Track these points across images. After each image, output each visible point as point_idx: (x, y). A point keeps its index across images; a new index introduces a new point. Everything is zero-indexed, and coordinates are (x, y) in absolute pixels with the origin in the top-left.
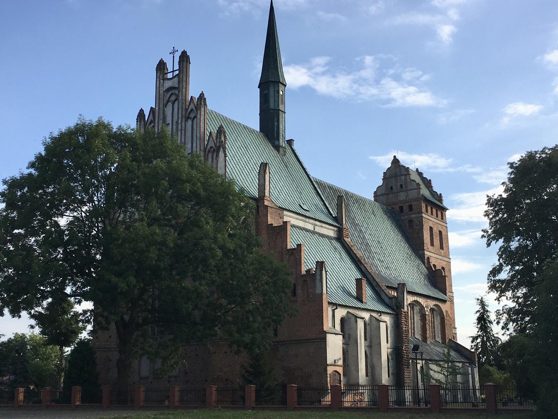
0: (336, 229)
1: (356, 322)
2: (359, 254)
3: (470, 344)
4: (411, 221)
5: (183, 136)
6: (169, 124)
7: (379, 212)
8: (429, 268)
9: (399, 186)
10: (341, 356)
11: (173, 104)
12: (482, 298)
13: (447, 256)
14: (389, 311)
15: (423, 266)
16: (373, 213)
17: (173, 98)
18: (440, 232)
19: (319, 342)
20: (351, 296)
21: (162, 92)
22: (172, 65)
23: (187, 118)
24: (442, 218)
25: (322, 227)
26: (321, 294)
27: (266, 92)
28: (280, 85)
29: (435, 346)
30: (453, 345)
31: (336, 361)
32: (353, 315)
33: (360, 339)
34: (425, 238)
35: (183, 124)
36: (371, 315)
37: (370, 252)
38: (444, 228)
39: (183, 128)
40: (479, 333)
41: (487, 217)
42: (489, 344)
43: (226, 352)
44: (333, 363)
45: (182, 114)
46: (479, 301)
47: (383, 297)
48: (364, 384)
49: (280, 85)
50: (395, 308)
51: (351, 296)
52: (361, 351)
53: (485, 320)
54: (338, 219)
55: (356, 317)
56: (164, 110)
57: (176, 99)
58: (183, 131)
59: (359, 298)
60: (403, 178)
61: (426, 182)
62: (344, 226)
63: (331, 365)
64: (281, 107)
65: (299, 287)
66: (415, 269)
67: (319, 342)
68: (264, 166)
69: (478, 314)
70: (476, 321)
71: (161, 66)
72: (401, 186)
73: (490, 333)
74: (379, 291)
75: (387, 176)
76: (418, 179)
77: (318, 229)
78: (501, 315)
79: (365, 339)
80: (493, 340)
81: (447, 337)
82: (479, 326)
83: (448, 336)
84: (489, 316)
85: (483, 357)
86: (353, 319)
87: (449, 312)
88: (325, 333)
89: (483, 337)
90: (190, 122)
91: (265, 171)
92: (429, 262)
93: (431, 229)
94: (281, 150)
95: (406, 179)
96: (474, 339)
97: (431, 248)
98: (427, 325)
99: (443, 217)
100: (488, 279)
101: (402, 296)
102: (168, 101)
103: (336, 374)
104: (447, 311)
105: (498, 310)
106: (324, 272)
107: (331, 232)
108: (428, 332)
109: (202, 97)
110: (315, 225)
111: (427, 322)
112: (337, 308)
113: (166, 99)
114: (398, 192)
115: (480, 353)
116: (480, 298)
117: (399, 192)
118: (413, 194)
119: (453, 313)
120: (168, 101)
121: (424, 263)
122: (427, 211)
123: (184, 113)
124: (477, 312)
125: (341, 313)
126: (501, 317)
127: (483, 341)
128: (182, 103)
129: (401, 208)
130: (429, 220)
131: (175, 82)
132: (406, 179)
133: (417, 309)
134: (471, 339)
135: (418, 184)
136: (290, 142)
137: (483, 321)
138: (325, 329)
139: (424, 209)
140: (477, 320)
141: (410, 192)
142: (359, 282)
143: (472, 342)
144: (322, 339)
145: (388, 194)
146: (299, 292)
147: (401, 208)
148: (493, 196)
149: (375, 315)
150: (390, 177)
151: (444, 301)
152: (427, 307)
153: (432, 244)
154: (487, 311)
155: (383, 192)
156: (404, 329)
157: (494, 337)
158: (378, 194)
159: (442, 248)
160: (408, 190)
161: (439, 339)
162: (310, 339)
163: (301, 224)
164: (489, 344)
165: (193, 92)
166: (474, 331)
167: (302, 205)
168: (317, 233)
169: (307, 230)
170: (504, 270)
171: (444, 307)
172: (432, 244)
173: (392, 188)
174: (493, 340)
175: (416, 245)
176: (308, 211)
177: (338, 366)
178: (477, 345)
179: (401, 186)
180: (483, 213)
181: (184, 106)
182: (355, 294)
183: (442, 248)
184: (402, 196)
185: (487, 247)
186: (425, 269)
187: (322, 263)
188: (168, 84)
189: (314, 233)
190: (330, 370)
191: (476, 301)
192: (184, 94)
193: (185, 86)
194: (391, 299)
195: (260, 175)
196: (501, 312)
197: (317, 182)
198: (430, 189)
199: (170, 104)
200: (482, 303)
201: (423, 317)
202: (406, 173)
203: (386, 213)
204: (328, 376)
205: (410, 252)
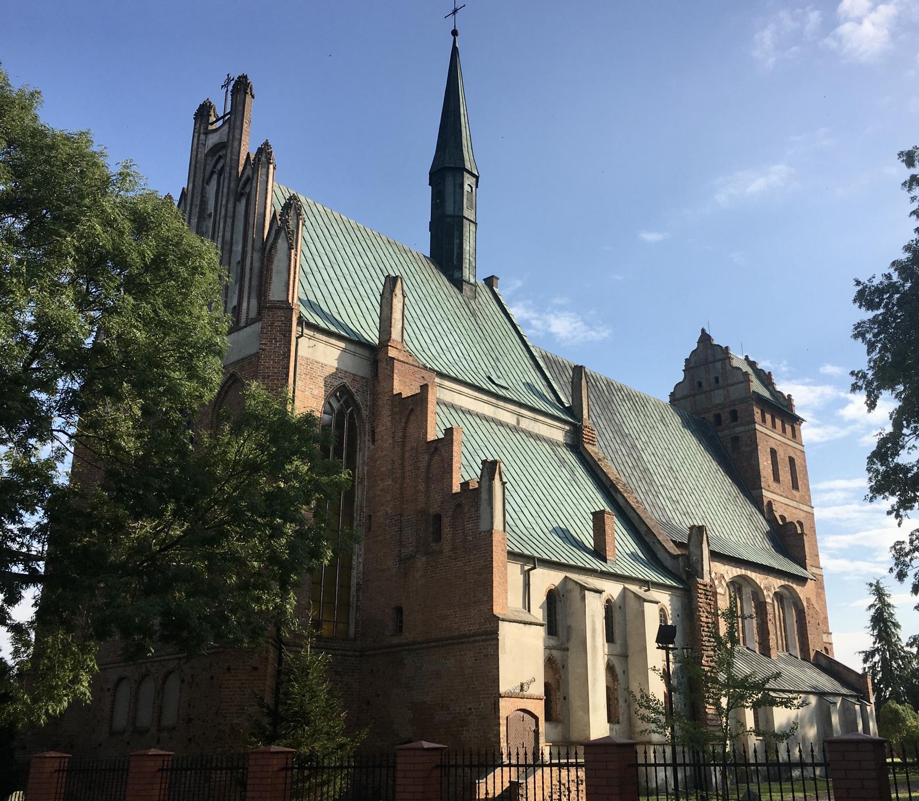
0: (567, 428)
1: (583, 598)
2: (611, 469)
3: (862, 665)
4: (736, 439)
5: (228, 229)
6: (210, 215)
7: (676, 421)
8: (770, 518)
9: (712, 379)
11: (220, 175)
12: (878, 582)
13: (807, 501)
14: (668, 582)
15: (761, 517)
16: (662, 419)
18: (792, 461)
19: (484, 641)
20: (580, 546)
21: (201, 156)
24: (794, 436)
25: (536, 420)
26: (490, 532)
28: (466, 175)
29: (787, 663)
30: (823, 662)
31: (525, 687)
32: (577, 583)
33: (594, 637)
34: (761, 467)
35: (230, 206)
36: (625, 588)
37: (651, 483)
38: (799, 453)
39: (230, 214)
40: (877, 645)
41: (860, 340)
42: (895, 665)
43: (255, 669)
44: (518, 691)
45: (229, 187)
46: (874, 588)
47: (661, 555)
49: (466, 175)
50: (684, 577)
51: (580, 546)
52: (594, 666)
53: (885, 621)
54: (574, 411)
55: (583, 588)
56: (203, 189)
58: (229, 220)
59: (599, 552)
60: (719, 365)
61: (764, 377)
62: (587, 422)
63: (510, 696)
64: (467, 213)
65: (446, 521)
66: (745, 522)
67: (484, 641)
68: (391, 282)
69: (873, 611)
70: (869, 624)
72: (717, 380)
73: (896, 645)
74: (651, 544)
75: (691, 365)
76: (746, 368)
77: (525, 424)
78: (907, 554)
80: (902, 658)
81: (811, 648)
82: (876, 632)
83: (815, 646)
84: (892, 614)
85: (887, 689)
86: (577, 592)
87: (814, 601)
88: (498, 619)
89: (884, 652)
91: (393, 291)
92: (771, 510)
93: (773, 453)
94: (466, 287)
95: (724, 368)
96: (868, 655)
97: (774, 485)
98: (770, 624)
99: (795, 435)
100: (869, 470)
101: (698, 552)
102: (213, 173)
103: (526, 716)
104: (808, 599)
105: (899, 543)
106: (497, 483)
107: (558, 434)
108: (772, 637)
111: (770, 617)
112: (534, 568)
113: (209, 169)
114: (711, 390)
115: (880, 682)
116: (874, 582)
117: (713, 390)
118: (735, 392)
119: (824, 606)
120: (213, 173)
121: (761, 512)
122: (764, 421)
123: (232, 185)
124: (870, 607)
125: (545, 580)
126: (907, 559)
127: (883, 659)
128: (231, 169)
129: (718, 417)
130: (768, 435)
132: (724, 368)
133: (747, 591)
134: (862, 656)
135: (746, 374)
136: (490, 282)
137: (882, 622)
138: (497, 610)
139: (758, 416)
140: (872, 621)
141: (732, 389)
142: (598, 518)
143: (865, 661)
144: (486, 633)
145: (694, 395)
146: (447, 530)
147: (718, 417)
148: (870, 280)
149: (634, 588)
151: (802, 580)
152: (769, 590)
153: (777, 479)
154: (889, 605)
156: (704, 619)
157: (904, 652)
158: (677, 396)
159: (795, 486)
160: (728, 386)
161: (798, 653)
162: (465, 636)
163: (487, 410)
164: (895, 665)
166: (868, 641)
167: (494, 378)
169: (500, 423)
170: (908, 445)
171: (804, 592)
172: (777, 479)
173: (700, 384)
174: (902, 658)
175: (746, 480)
176: (507, 389)
178: (873, 667)
179: (717, 380)
180: (850, 331)
181: (234, 172)
182: (589, 542)
183: (795, 486)
184: (718, 397)
185: (869, 411)
186: (764, 523)
187: (495, 463)
188: (213, 140)
189: (516, 429)
190: (507, 708)
191: (868, 587)
192: (235, 150)
193: (237, 137)
194: (678, 561)
195: (384, 301)
196: (907, 547)
197: (545, 358)
198: (771, 388)
199: (215, 176)
200: (879, 592)
201: (761, 607)
203: (687, 424)
204: (503, 722)
205: (734, 490)
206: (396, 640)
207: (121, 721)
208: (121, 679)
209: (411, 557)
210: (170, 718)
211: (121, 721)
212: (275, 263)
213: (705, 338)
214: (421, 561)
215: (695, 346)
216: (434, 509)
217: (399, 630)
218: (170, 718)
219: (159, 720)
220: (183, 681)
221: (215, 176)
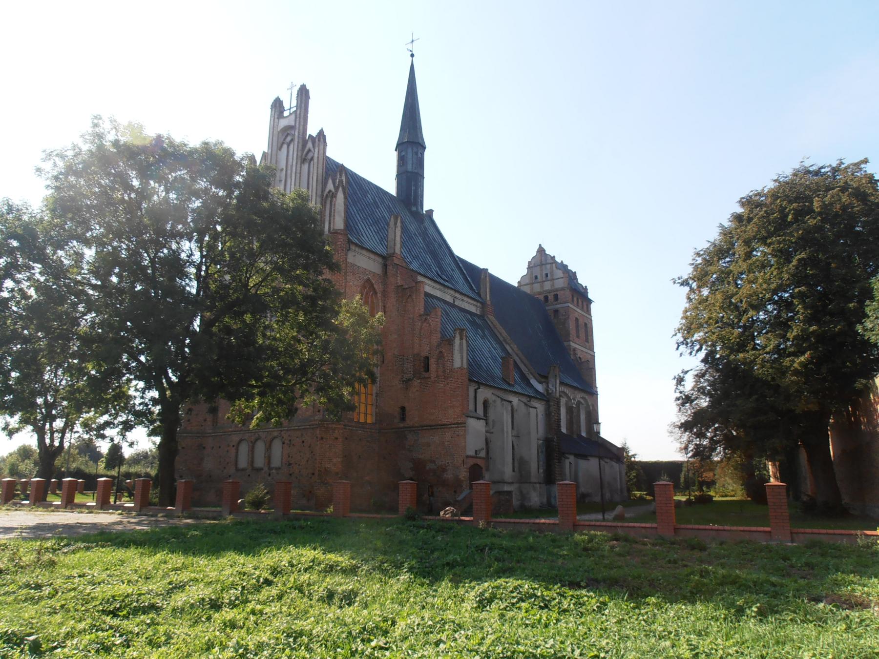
0: (479, 304)
4: (556, 311)
6: (282, 170)
10: (484, 446)
17: (289, 139)
18: (586, 324)
22: (290, 103)
23: (304, 161)
25: (463, 300)
27: (403, 153)
35: (298, 169)
39: (298, 171)
48: (510, 481)
57: (292, 140)
58: (298, 175)
60: (548, 266)
71: (277, 105)
72: (547, 275)
79: (513, 428)
90: (306, 166)
93: (577, 319)
102: (283, 143)
109: (321, 134)
110: (455, 298)
113: (281, 140)
123: (300, 154)
129: (546, 298)
131: (291, 122)
147: (546, 298)
150: (535, 266)
153: (578, 337)
155: (527, 281)
158: (523, 283)
165: (312, 130)
168: (457, 306)
173: (536, 277)
177: (480, 458)
179: (547, 275)
184: (547, 286)
188: (283, 123)
199: (285, 146)
202: (390, 623)
206: (402, 425)
207: (243, 463)
208: (241, 441)
209: (409, 380)
210: (276, 462)
211: (243, 463)
212: (337, 206)
213: (541, 250)
214: (416, 382)
215: (535, 254)
216: (425, 353)
217: (403, 419)
218: (276, 462)
219: (269, 462)
220: (284, 443)
221: (285, 146)
